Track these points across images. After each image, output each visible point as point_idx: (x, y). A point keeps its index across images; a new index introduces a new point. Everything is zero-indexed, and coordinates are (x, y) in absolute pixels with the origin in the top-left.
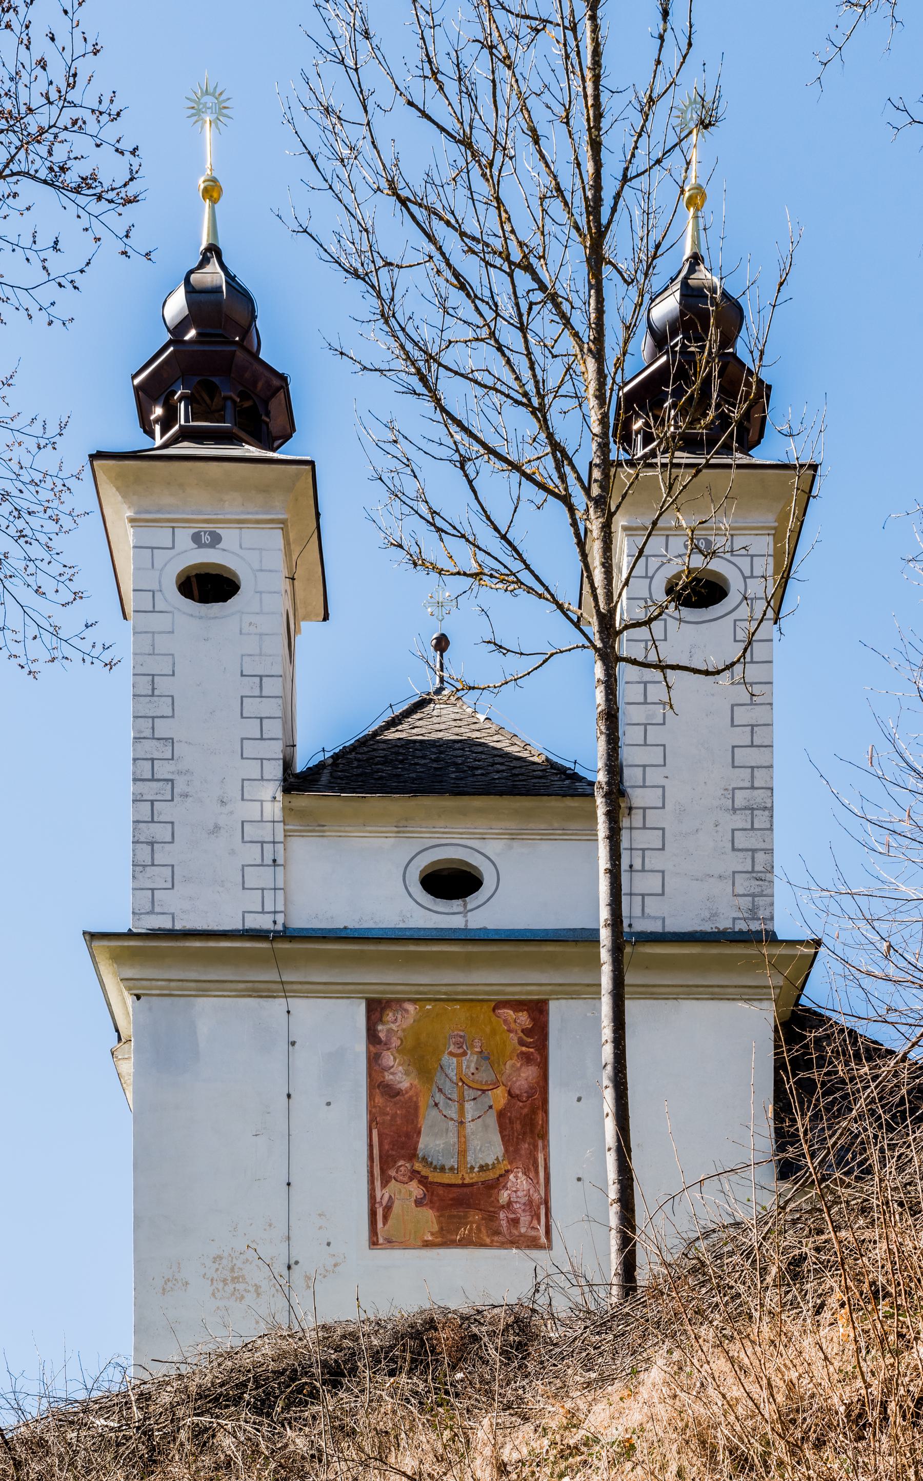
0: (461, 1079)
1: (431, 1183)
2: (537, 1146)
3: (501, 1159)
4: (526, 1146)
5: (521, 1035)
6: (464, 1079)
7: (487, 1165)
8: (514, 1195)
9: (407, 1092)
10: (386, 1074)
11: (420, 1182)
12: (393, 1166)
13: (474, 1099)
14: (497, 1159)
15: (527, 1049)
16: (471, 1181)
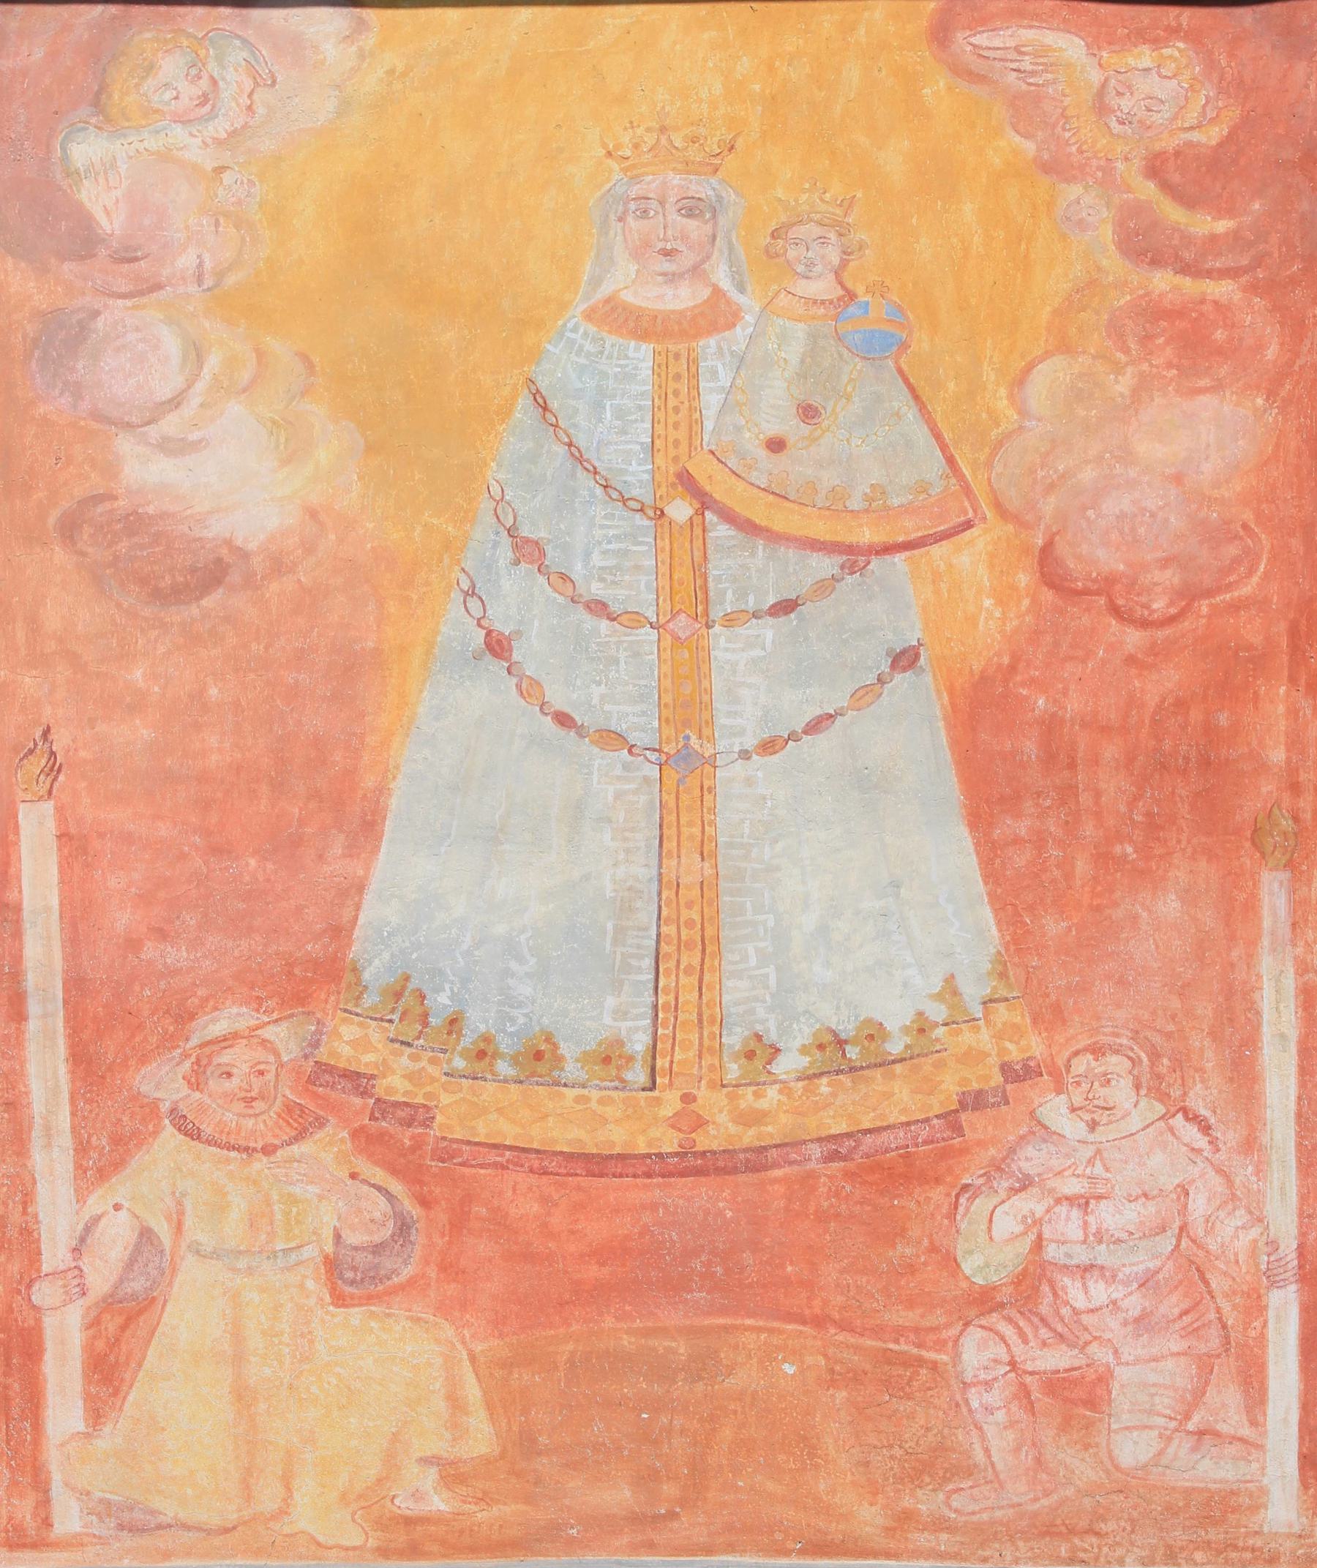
0: (686, 482)
1: (447, 1152)
2: (1251, 907)
3: (973, 992)
4: (1170, 906)
5: (1148, 190)
6: (702, 470)
7: (874, 1033)
8: (1069, 1224)
9: (309, 548)
10: (125, 445)
11: (367, 1141)
12: (169, 1041)
13: (786, 607)
14: (950, 990)
15: (1188, 285)
16: (749, 1137)
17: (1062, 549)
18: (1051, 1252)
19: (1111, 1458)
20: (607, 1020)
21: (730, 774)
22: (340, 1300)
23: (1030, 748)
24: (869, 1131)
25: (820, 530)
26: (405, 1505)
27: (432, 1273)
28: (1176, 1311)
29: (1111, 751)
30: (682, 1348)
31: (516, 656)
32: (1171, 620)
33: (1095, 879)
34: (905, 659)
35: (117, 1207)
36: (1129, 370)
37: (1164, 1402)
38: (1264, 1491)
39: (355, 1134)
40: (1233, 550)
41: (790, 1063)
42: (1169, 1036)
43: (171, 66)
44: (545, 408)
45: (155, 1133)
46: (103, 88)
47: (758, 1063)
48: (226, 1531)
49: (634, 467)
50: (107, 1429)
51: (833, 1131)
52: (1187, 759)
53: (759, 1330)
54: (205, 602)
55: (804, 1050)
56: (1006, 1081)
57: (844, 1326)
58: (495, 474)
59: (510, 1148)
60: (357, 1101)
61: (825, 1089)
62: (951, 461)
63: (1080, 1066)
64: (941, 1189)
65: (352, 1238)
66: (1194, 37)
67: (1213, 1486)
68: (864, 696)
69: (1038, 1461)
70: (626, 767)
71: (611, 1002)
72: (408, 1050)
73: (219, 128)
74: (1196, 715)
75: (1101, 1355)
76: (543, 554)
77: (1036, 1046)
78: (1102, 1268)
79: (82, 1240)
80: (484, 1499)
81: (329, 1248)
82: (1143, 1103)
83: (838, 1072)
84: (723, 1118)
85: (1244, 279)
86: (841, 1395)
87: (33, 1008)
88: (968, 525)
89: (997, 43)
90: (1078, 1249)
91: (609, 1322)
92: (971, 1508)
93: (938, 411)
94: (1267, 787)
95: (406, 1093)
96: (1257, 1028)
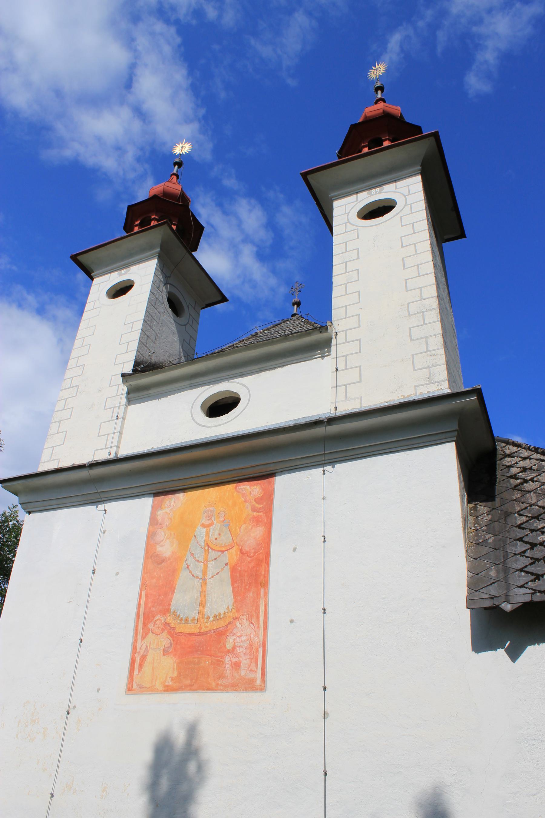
0: (207, 545)
2: (260, 594)
4: (251, 594)
7: (220, 614)
8: (238, 640)
11: (169, 633)
13: (215, 559)
16: (206, 630)
17: (243, 548)
18: (236, 644)
19: (240, 674)
20: (194, 614)
21: (208, 581)
22: (164, 655)
23: (238, 575)
24: (218, 628)
25: (219, 549)
26: (167, 684)
27: (173, 650)
28: (249, 652)
29: (246, 574)
30: (196, 660)
31: (189, 568)
32: (253, 556)
33: (244, 591)
34: (226, 564)
35: (145, 643)
36: (251, 525)
37: (247, 666)
38: (257, 679)
39: (168, 632)
40: (260, 547)
41: (211, 619)
42: (250, 612)
43: (167, 502)
44: (195, 537)
45: (149, 633)
46: (161, 505)
47: (208, 619)
48: (149, 688)
49: (203, 543)
50: (140, 673)
51: (214, 628)
52: (254, 574)
53: (205, 657)
54: (162, 564)
55: (213, 617)
56: (233, 620)
57: (214, 656)
58: (190, 546)
59: (182, 633)
60: (169, 627)
61: (214, 623)
62: (233, 539)
63: (241, 617)
64: (225, 636)
65: (166, 646)
66: (260, 484)
67: (251, 678)
68: (222, 569)
69: (232, 675)
70: (199, 581)
71: (194, 612)
72: (174, 620)
73: (170, 508)
74: (255, 569)
75: (240, 659)
76: (193, 555)
77: (236, 615)
78: (241, 646)
79: (141, 647)
80: (175, 683)
81: (164, 647)
82: (247, 622)
83: (216, 620)
84: (204, 627)
85: (263, 512)
86: (212, 666)
87: (140, 617)
88: (234, 547)
89: (241, 488)
90: (239, 643)
91: (190, 657)
92: (225, 682)
93: (232, 533)
94: (262, 577)
95: (174, 626)
96: (260, 611)
